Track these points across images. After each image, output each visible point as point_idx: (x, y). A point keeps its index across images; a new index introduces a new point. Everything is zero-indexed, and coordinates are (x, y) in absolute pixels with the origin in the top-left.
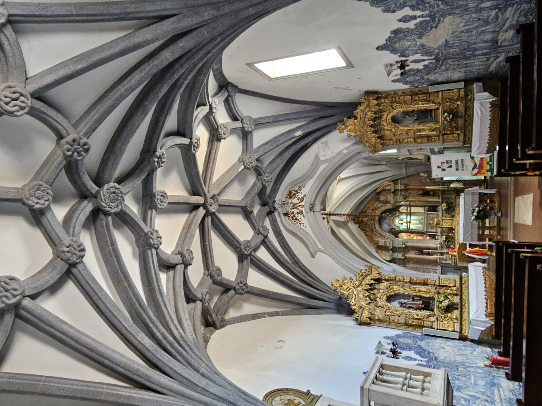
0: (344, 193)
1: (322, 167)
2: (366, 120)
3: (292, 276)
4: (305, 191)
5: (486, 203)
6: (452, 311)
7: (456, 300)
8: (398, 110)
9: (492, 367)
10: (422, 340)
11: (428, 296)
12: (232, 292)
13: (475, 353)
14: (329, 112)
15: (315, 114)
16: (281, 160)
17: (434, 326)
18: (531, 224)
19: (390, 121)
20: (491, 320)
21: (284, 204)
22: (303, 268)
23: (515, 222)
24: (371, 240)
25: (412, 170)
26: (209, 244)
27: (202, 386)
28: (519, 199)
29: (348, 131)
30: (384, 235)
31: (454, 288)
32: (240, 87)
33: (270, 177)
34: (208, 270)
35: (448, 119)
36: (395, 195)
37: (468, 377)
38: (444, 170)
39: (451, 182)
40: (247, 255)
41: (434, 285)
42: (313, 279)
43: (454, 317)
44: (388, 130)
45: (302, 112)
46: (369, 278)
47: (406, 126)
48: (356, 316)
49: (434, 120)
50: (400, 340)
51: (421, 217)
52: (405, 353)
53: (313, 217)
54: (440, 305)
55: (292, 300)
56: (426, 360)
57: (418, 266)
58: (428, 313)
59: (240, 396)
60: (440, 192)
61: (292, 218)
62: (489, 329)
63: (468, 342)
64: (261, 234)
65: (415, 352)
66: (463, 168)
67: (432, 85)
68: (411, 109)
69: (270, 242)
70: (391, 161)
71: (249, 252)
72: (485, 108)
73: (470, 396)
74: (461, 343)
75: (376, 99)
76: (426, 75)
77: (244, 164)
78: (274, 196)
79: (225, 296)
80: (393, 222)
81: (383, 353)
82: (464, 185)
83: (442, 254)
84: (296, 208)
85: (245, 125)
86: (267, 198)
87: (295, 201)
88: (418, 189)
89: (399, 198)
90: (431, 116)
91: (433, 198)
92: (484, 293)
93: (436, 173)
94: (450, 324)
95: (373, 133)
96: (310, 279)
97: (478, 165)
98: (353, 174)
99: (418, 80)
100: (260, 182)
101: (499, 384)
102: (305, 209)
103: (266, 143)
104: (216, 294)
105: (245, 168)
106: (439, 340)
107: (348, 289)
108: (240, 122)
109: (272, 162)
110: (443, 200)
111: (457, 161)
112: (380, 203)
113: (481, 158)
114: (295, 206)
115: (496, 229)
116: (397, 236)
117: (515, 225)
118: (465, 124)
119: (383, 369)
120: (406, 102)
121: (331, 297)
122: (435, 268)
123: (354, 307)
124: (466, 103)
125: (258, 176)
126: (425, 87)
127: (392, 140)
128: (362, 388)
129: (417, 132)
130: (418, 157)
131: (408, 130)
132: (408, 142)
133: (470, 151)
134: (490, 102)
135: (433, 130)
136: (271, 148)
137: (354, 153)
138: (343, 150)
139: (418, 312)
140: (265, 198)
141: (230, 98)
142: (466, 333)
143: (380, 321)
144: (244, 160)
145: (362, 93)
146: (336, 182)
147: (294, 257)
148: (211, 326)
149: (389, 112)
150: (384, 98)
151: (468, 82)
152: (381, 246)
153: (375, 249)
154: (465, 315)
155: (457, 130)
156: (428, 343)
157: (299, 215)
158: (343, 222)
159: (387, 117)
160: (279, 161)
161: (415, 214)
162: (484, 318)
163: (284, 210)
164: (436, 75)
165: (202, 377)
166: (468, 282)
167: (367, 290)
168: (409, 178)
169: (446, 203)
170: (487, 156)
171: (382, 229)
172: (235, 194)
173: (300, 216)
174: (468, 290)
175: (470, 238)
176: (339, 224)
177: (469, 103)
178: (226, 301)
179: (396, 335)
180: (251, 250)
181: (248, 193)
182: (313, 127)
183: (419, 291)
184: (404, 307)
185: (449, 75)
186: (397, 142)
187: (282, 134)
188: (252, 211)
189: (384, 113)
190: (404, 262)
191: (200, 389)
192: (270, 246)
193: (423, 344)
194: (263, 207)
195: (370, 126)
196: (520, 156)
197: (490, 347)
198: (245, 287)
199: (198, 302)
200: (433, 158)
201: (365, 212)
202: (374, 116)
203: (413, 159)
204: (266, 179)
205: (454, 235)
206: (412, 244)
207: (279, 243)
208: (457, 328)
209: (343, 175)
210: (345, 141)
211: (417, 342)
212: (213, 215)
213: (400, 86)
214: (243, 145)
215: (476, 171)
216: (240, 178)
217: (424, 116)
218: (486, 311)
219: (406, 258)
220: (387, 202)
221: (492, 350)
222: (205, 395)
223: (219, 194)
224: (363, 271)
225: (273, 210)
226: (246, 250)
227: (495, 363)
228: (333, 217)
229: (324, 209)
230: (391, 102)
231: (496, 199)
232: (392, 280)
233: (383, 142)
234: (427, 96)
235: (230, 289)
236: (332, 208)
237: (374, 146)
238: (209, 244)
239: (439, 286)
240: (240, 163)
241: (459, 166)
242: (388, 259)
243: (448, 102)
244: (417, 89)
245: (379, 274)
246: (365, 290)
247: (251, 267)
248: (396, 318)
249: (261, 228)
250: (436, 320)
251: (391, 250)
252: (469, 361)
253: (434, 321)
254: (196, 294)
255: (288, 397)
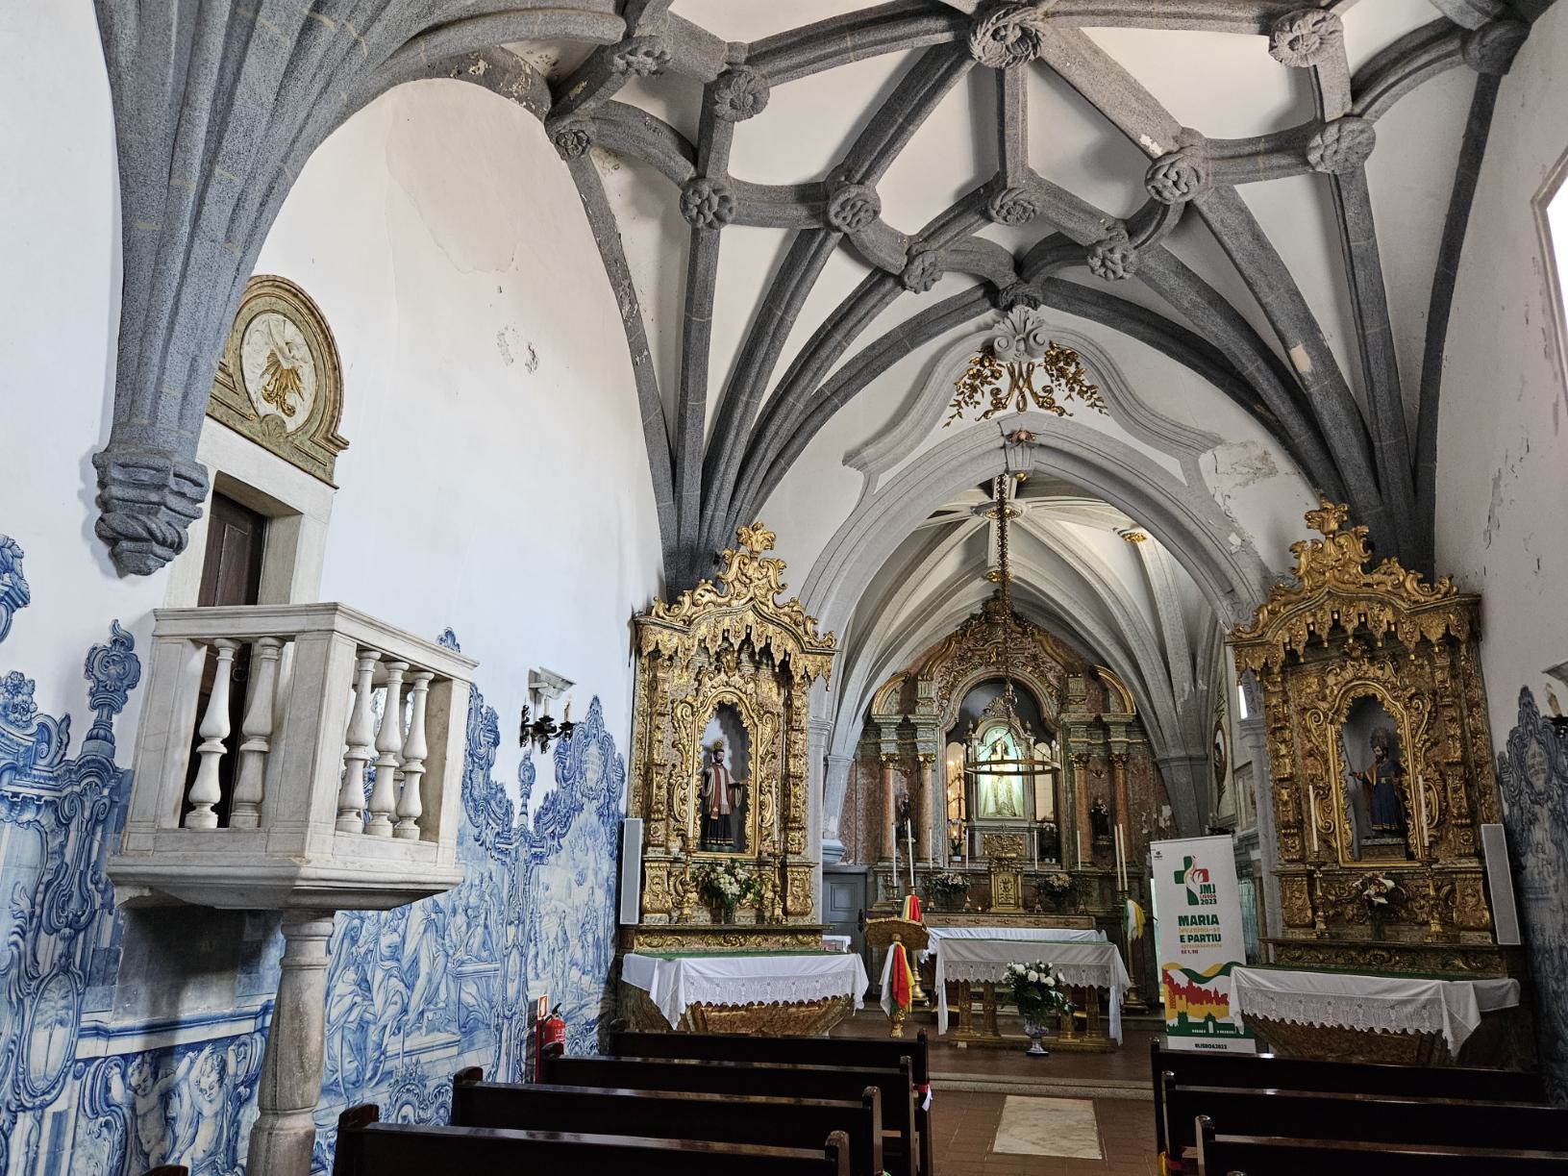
0: (1085, 557)
1: (1171, 464)
2: (1362, 606)
3: (775, 393)
4: (1079, 409)
5: (1072, 1009)
6: (708, 904)
7: (744, 917)
8: (1404, 720)
9: (530, 1026)
10: (601, 815)
11: (748, 831)
12: (688, 171)
13: (575, 973)
14: (1393, 470)
15: (1384, 414)
16: (1195, 305)
17: (651, 853)
18: (997, 1149)
19: (1361, 692)
20: (683, 1017)
21: (1025, 340)
22: (808, 429)
23: (1011, 1100)
24: (934, 656)
25: (1180, 777)
26: (846, 50)
27: (261, 20)
28: (1084, 1111)
29: (1315, 542)
30: (955, 693)
31: (778, 912)
32: (1505, 79)
33: (1123, 271)
34: (749, 61)
35: (1371, 891)
36: (1089, 725)
37: (485, 954)
38: (1179, 877)
39: (1145, 902)
40: (826, 213)
41: (786, 851)
42: (773, 464)
43: (686, 911)
44: (1323, 684)
45: (1391, 364)
46: (790, 645)
47: (1341, 750)
48: (660, 608)
49: (1364, 842)
50: (594, 749)
51: (1019, 810)
52: (545, 764)
53: (985, 448)
54: (720, 869)
55: (691, 395)
56: (531, 827)
57: (861, 804)
58: (693, 830)
59: (251, 177)
60: (1108, 869)
61: (978, 375)
62: (654, 1015)
63: (611, 953)
64: (910, 262)
65: (555, 795)
66: (1190, 938)
67: (1509, 833)
68: (1408, 761)
69: (883, 302)
70: (1208, 711)
71: (836, 222)
72: (1417, 1013)
73: (415, 961)
74: (604, 928)
75: (1447, 635)
76: (1552, 811)
77: (1169, 153)
78: (1056, 299)
79: (668, 143)
80: (997, 724)
81: (535, 694)
82: (1134, 942)
83: (904, 874)
84: (1014, 385)
85: (1333, 130)
86: (1046, 272)
87: (1040, 379)
88: (1114, 799)
89: (1079, 741)
90: (1382, 833)
91: (1088, 846)
92: (768, 1001)
93: (1166, 855)
94: (657, 897)
95: (1311, 633)
96: (771, 456)
97: (1203, 987)
98: (1156, 584)
99: (1530, 784)
100: (1103, 235)
101: (471, 1044)
102: (1011, 417)
103: (1258, 237)
104: (672, 105)
105: (1155, 161)
106: (607, 866)
107: (747, 581)
108: (1347, 110)
109: (1183, 270)
110: (1082, 876)
111: (1215, 920)
112: (1059, 679)
113: (1225, 996)
114: (1020, 379)
115: (990, 1035)
116: (951, 737)
117: (1000, 1097)
118: (1353, 946)
119: (432, 683)
120: (1435, 744)
121: (718, 528)
122: (860, 855)
123: (687, 600)
124: (1435, 951)
125: (1125, 222)
126: (1500, 810)
127: (1285, 702)
128: (333, 608)
129: (1316, 788)
130: (1227, 796)
131: (1324, 754)
132: (1277, 756)
133: (1252, 961)
134: (1440, 1031)
135: (1324, 840)
136: (1238, 256)
137: (1230, 573)
138: (1239, 535)
139: (693, 802)
140: (1046, 265)
141: (1455, 44)
142: (640, 943)
143: (653, 685)
144: (1188, 152)
145: (1473, 584)
146: (1124, 522)
147: (842, 394)
148: (554, 103)
149: (1394, 688)
150: (1452, 665)
151: (1522, 960)
152: (916, 688)
153: (903, 668)
154: (696, 944)
155: (1327, 920)
156: (593, 833)
157: (989, 398)
158: (985, 561)
159: (1377, 679)
160: (1190, 297)
161: (1031, 790)
162: (686, 998)
163: (1004, 343)
164: (1549, 846)
165: (297, 25)
166: (801, 953)
167: (748, 639)
168: (1150, 772)
169: (1073, 887)
170: (1233, 1015)
171: (972, 688)
172: (1049, 137)
173: (986, 402)
174: (777, 953)
175: (955, 958)
176: (976, 544)
177: (1434, 962)
178: (651, 150)
179: (608, 737)
180: (845, 229)
181: (1058, 194)
182: (1330, 411)
183: (762, 805)
184: (707, 759)
185: (1552, 894)
186: (1277, 720)
187: (1298, 294)
188: (990, 220)
189: (1389, 668)
190: (869, 759)
191: (250, 15)
192: (872, 301)
193: (588, 816)
194: (1008, 261)
195: (1336, 622)
196: (1219, 1138)
197: (601, 1017)
198: (710, 217)
199: (621, 26)
200: (1224, 844)
201: (1024, 633)
202: (1379, 634)
203: (1221, 778)
204: (1117, 256)
205: (968, 911)
206: (929, 786)
207: (886, 336)
208: (652, 920)
209: (1151, 548)
210: (1277, 538)
211: (591, 799)
212: (960, 50)
213: (1503, 720)
214: (1250, 141)
215: (1182, 981)
216: (1117, 150)
217: (1383, 807)
218: (709, 1004)
219: (883, 766)
220: (1064, 701)
221: (594, 1022)
222: (228, 35)
223: (1042, 66)
224: (809, 626)
225: (1003, 303)
226: (843, 207)
227: (542, 1034)
228: (995, 524)
229: (1022, 490)
230: (1435, 693)
231: (1090, 1041)
232: (789, 721)
233: (1276, 670)
234: (1460, 816)
235: (695, 163)
236: (1028, 519)
237: (1259, 643)
238: (846, 50)
239: (784, 866)
240: (1176, 139)
241: (1198, 927)
242: (874, 711)
243: (1438, 889)
244: (1493, 782)
245: (806, 676)
246: (748, 635)
247: (786, 238)
248: (665, 735)
249: (929, 258)
250: (671, 857)
251: (906, 720)
252: (544, 954)
253: (668, 852)
254: (648, 10)
255: (306, 371)
